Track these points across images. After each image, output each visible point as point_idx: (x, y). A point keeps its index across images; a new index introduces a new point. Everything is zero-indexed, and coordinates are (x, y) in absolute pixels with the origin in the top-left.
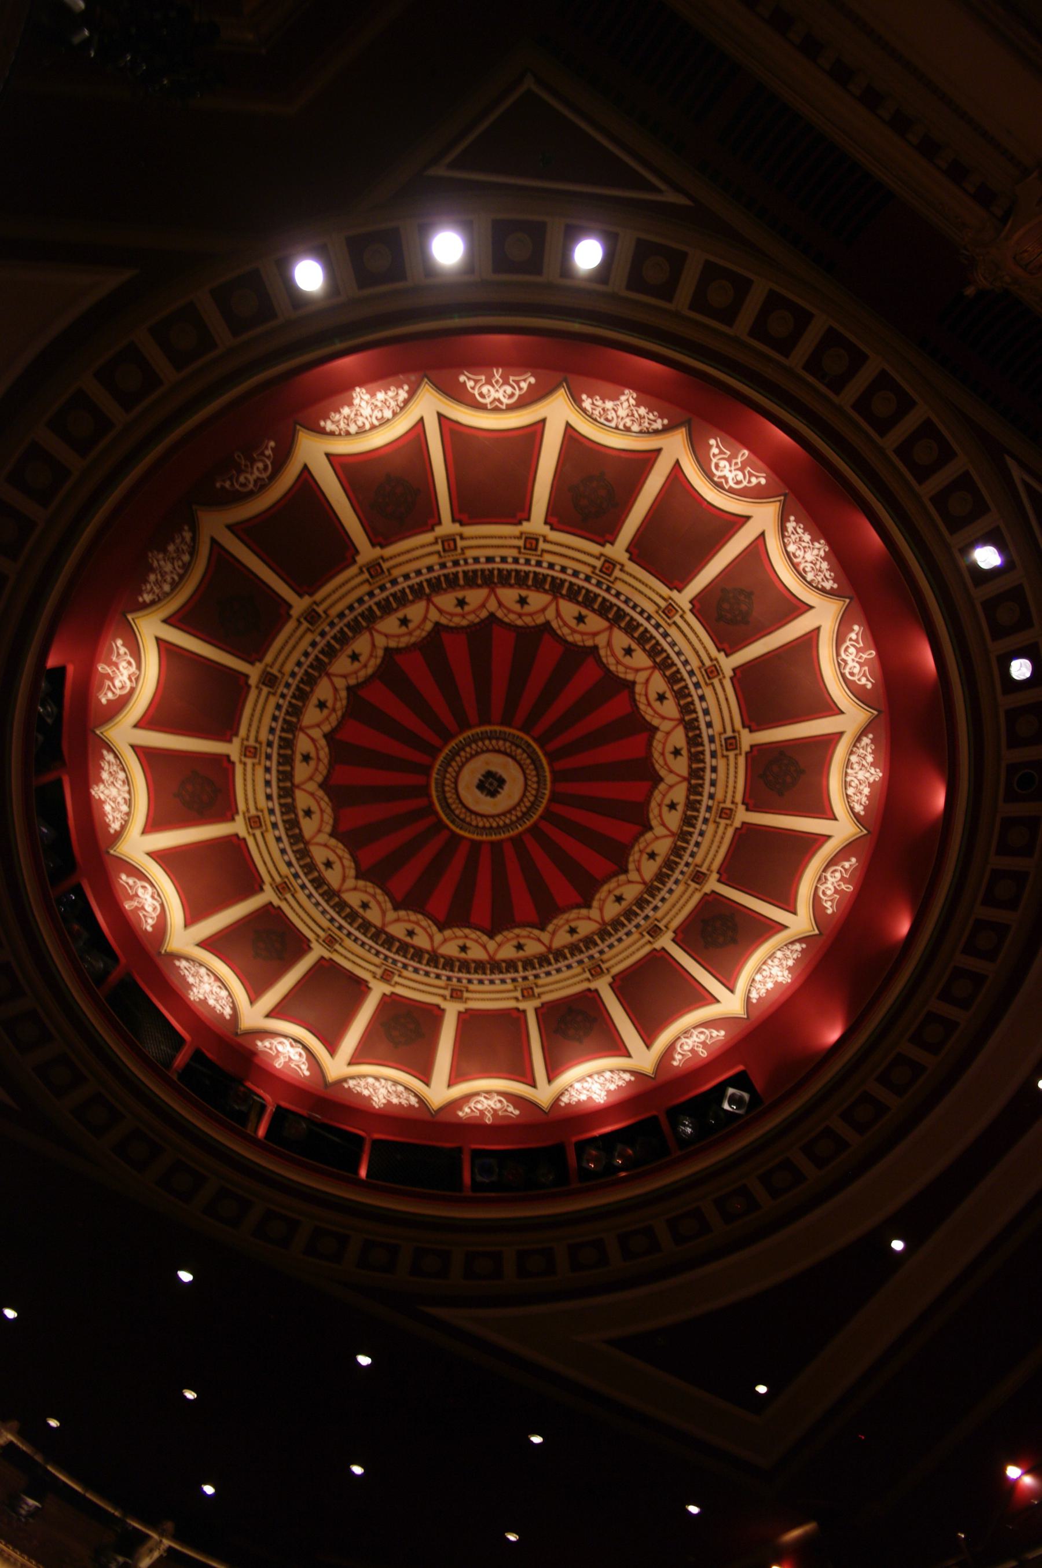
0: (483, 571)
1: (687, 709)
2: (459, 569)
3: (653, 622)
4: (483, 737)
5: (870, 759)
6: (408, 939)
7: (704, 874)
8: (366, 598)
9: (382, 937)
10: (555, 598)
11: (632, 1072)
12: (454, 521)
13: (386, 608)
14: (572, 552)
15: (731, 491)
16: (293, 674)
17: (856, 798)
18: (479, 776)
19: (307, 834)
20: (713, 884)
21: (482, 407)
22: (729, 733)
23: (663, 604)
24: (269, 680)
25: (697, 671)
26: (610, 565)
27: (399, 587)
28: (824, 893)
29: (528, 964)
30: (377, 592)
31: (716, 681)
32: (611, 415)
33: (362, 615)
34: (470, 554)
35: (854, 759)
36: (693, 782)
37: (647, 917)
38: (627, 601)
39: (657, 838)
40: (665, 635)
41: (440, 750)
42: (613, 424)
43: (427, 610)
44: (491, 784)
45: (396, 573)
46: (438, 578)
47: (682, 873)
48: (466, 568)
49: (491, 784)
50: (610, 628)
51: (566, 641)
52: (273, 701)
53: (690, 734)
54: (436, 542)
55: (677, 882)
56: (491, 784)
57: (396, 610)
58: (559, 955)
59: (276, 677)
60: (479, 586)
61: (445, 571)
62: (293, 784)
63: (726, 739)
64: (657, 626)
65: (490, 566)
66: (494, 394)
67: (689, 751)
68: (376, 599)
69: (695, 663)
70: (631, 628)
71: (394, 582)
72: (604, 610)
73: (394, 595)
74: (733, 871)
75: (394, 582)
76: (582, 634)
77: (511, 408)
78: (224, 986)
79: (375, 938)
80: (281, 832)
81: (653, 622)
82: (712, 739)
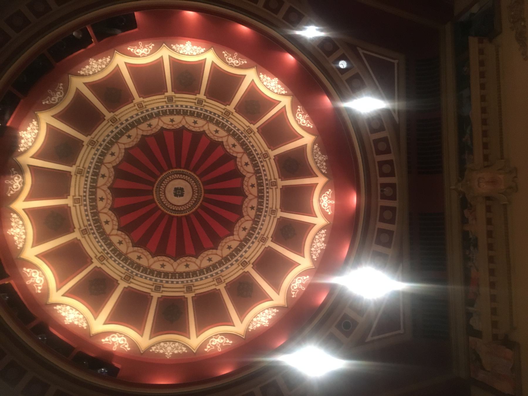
0: (248, 146)
1: (111, 143)
2: (244, 139)
3: (87, 175)
4: (194, 179)
5: (87, 67)
6: (256, 185)
7: (168, 98)
8: (217, 115)
9: (93, 189)
10: (254, 173)
11: (259, 75)
12: (257, 128)
13: (217, 123)
14: (271, 170)
15: (320, 205)
16: (177, 106)
17: (105, 63)
18: (179, 186)
19: (237, 243)
20: (170, 93)
21: (295, 117)
22: (111, 123)
23: (274, 209)
24: (189, 289)
25: (260, 234)
26: (275, 184)
27: (227, 124)
28: (148, 51)
29: (115, 251)
30: (221, 118)
31: (95, 140)
32: (317, 155)
33: (211, 117)
34: (100, 250)
35: (91, 73)
36: (136, 124)
37: (161, 281)
38: (268, 196)
39: (195, 263)
40: (90, 168)
41: (180, 168)
42: (315, 158)
43: (130, 252)
44: (179, 192)
45: (230, 120)
46: (237, 134)
47: (187, 281)
48: (245, 140)
49: (179, 192)
50: (99, 187)
51: (243, 186)
52: (196, 283)
53: (239, 248)
54: (247, 127)
55: (182, 282)
56: (179, 192)
57: (219, 127)
58: (126, 259)
59: (187, 287)
60: (243, 148)
61: (241, 135)
62: (223, 259)
63: (245, 261)
64: (88, 172)
65: (251, 148)
66: (300, 118)
67: (126, 133)
68: (218, 119)
69: (93, 151)
70: (260, 204)
71: (128, 270)
72: (260, 191)
73: (223, 123)
74: (160, 89)
75: (227, 121)
76: (248, 189)
77: (300, 126)
78: (314, 238)
79: (92, 187)
80: (116, 131)
81: (87, 175)
82: (241, 256)
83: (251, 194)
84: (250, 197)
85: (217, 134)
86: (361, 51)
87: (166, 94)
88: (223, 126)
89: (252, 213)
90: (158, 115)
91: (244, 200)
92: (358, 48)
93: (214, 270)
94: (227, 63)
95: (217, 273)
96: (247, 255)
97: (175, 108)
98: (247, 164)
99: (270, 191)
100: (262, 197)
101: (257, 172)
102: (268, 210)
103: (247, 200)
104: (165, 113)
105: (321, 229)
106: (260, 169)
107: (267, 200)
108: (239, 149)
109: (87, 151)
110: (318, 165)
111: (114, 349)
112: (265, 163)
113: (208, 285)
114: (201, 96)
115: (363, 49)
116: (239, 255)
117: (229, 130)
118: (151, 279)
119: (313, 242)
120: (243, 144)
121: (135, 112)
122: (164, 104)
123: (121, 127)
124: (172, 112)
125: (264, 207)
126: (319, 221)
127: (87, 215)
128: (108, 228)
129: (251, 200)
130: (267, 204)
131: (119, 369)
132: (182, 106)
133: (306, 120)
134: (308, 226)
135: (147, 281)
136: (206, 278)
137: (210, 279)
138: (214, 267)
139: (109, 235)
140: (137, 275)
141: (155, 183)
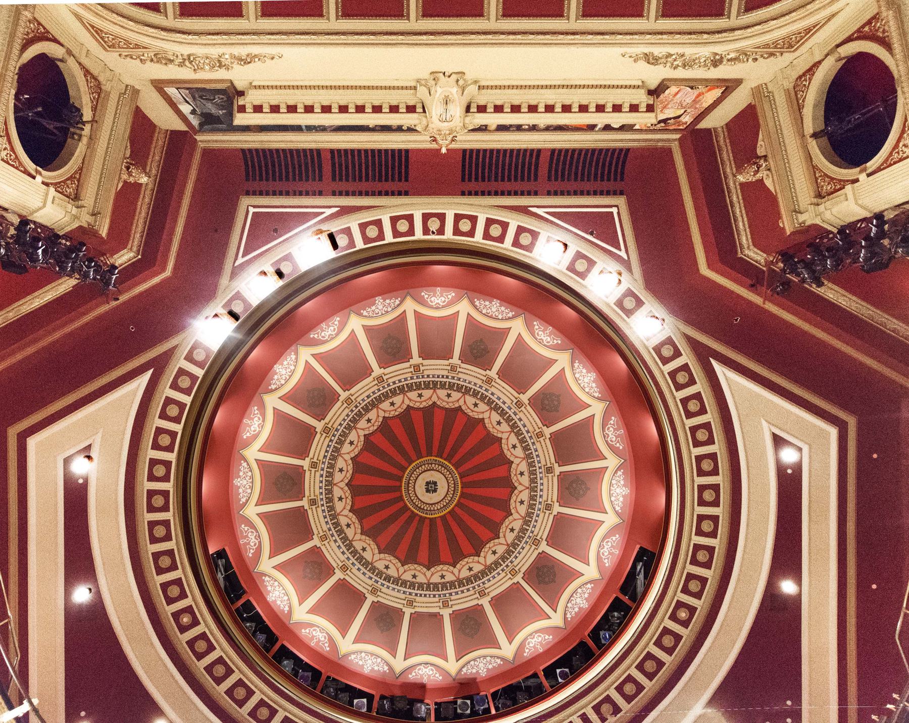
1: (373, 569)
13: (341, 442)
14: (399, 372)
18: (424, 487)
22: (515, 401)
31: (493, 383)
32: (377, 311)
40: (404, 592)
44: (431, 487)
45: (335, 426)
56: (431, 487)
64: (410, 594)
66: (327, 334)
70: (443, 386)
73: (340, 435)
79: (428, 588)
80: (358, 565)
83: (430, 398)
84: (435, 399)
85: (355, 443)
86: (240, 260)
87: (306, 507)
88: (345, 435)
89: (456, 395)
90: (334, 517)
91: (439, 407)
92: (237, 264)
93: (337, 532)
94: (603, 541)
95: (531, 437)
96: (508, 402)
97: (323, 496)
98: (392, 404)
99: (426, 373)
100: (435, 384)
101: (402, 390)
102: (450, 375)
103: (438, 403)
104: (332, 508)
105: (475, 307)
106: (398, 387)
107: (425, 595)
108: (372, 415)
109: (479, 376)
110: (390, 309)
111: (617, 552)
112: (472, 592)
113: (545, 448)
114: (305, 463)
115: (236, 259)
116: (508, 410)
117: (349, 428)
118: (538, 516)
119: (372, 654)
120: (367, 409)
121: (332, 543)
122: (320, 510)
123: (353, 560)
124: (532, 473)
125: (416, 592)
126: (464, 308)
127: (462, 592)
128: (477, 568)
129: (439, 398)
130: (443, 377)
131: (641, 548)
132: (321, 488)
133: (329, 326)
134: (471, 321)
135: (540, 520)
136: (536, 450)
137: (538, 445)
138: (341, 532)
139: (485, 566)
140: (532, 532)
141: (441, 457)
